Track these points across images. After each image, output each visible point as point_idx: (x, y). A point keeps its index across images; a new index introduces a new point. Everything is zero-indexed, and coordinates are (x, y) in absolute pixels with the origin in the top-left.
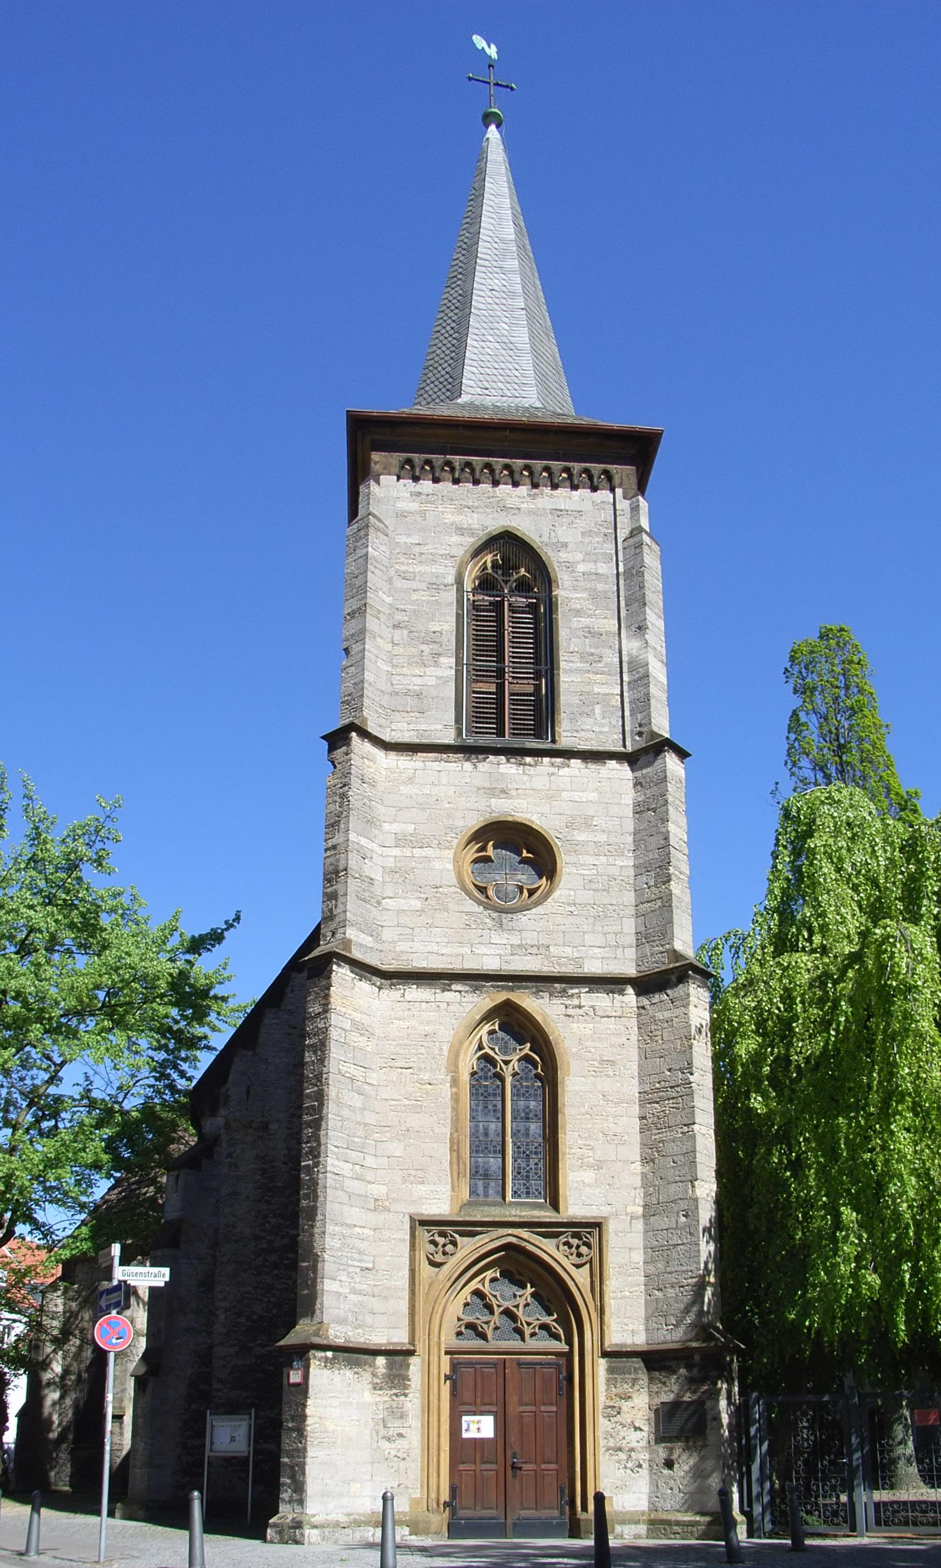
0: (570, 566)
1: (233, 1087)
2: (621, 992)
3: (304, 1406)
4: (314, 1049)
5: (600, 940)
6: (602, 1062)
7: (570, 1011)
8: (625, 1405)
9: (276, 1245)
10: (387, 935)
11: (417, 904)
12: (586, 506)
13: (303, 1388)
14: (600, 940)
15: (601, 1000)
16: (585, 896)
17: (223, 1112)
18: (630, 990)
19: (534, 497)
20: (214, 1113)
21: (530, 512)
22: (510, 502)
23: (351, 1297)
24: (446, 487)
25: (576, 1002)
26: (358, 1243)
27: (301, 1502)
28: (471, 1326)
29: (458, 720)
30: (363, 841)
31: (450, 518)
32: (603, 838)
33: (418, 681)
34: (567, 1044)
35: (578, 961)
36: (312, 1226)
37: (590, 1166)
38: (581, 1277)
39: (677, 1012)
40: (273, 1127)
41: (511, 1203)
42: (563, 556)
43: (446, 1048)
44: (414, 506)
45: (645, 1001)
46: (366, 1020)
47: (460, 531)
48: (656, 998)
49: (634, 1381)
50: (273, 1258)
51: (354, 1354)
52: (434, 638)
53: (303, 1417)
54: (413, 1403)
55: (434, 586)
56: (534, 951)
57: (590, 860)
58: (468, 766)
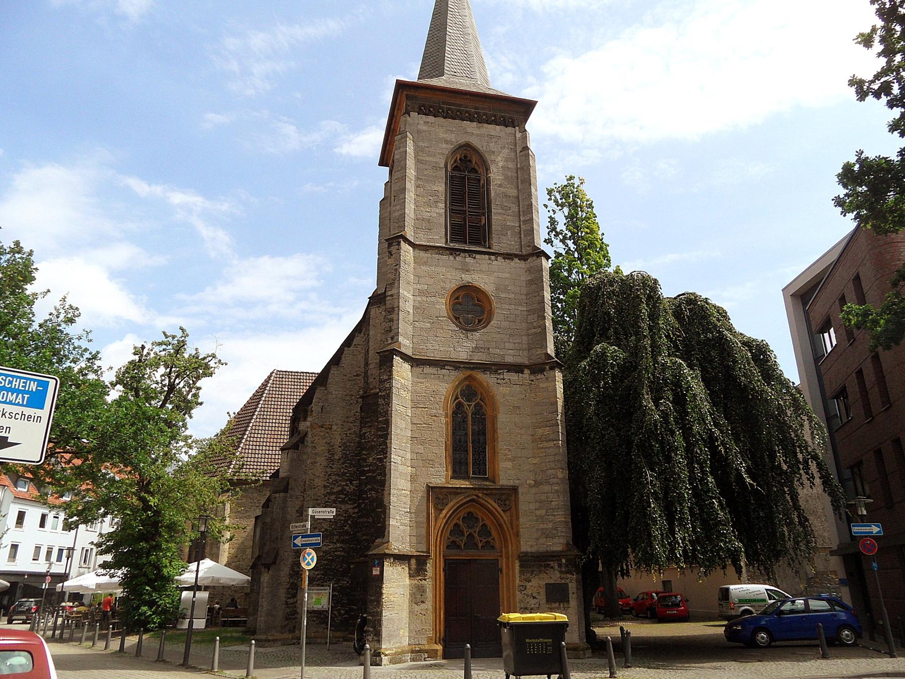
1: (315, 406)
2: (522, 372)
3: (381, 588)
4: (384, 397)
5: (511, 346)
6: (514, 407)
7: (499, 381)
8: (528, 585)
9: (335, 491)
12: (502, 134)
13: (380, 578)
14: (511, 346)
15: (514, 377)
16: (505, 324)
17: (309, 419)
18: (526, 371)
19: (479, 128)
20: (305, 420)
21: (477, 135)
22: (469, 130)
24: (440, 120)
25: (502, 377)
27: (379, 641)
28: (453, 542)
29: (446, 235)
30: (405, 293)
31: (442, 135)
32: (512, 296)
34: (498, 398)
35: (503, 356)
36: (383, 490)
37: (510, 460)
38: (505, 517)
39: (549, 384)
40: (334, 427)
42: (493, 157)
43: (443, 398)
44: (425, 128)
45: (532, 377)
47: (447, 142)
48: (539, 376)
49: (532, 572)
50: (333, 497)
51: (400, 558)
52: (435, 194)
53: (381, 594)
54: (428, 584)
55: (435, 168)
56: (482, 350)
57: (507, 307)
58: (451, 258)
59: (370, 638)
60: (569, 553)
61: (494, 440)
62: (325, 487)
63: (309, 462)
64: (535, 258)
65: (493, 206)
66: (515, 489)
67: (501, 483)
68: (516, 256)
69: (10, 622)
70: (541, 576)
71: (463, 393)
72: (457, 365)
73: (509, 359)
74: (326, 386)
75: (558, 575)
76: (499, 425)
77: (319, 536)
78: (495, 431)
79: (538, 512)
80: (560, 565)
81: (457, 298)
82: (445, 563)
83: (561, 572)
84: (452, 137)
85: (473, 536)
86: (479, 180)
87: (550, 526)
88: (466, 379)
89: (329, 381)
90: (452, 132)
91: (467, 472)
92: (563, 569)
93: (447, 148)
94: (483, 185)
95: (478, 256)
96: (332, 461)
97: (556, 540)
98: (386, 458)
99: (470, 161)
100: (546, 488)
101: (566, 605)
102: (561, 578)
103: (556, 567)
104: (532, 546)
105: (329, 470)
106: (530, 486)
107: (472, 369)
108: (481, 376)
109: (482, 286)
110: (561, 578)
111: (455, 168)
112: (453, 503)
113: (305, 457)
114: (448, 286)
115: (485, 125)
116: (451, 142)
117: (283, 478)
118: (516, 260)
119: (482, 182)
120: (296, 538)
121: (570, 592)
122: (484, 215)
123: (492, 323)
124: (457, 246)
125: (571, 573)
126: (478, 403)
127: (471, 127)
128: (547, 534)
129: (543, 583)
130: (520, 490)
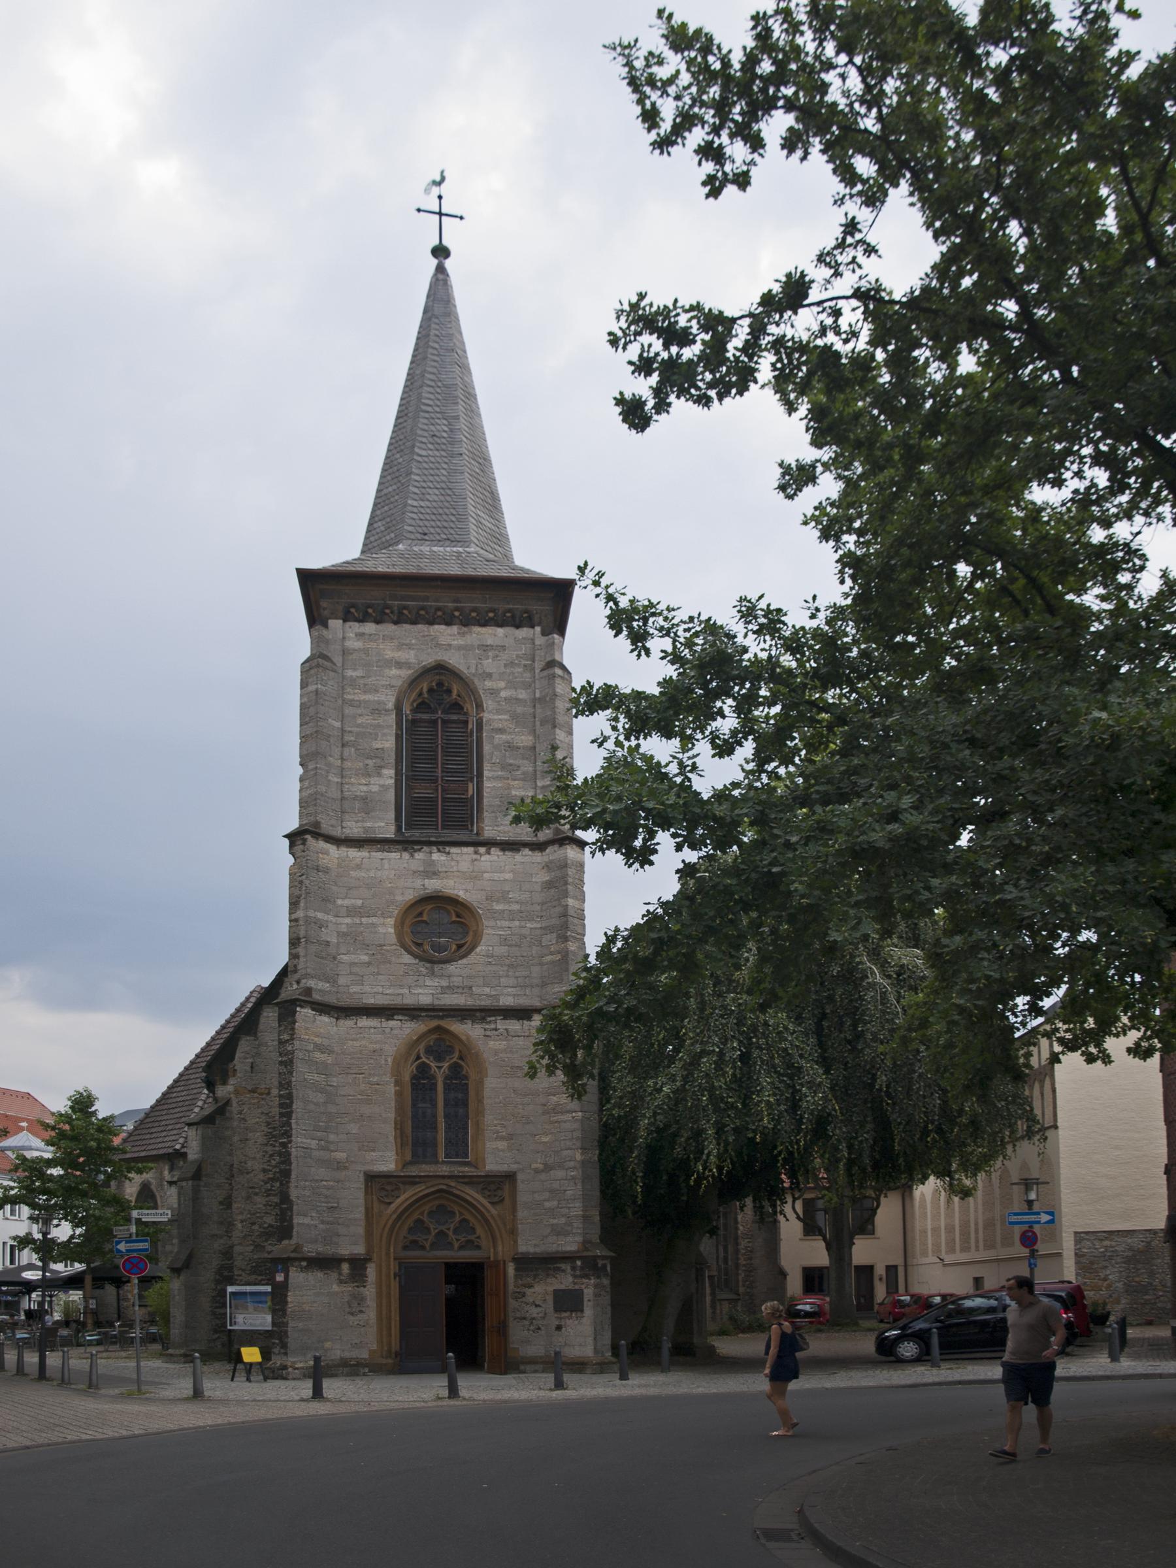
0: (494, 692)
1: (241, 1061)
5: (512, 981)
7: (488, 1033)
8: (529, 1291)
10: (342, 981)
11: (365, 958)
14: (512, 981)
15: (514, 1025)
16: (502, 950)
17: (232, 1081)
19: (463, 634)
20: (225, 1083)
21: (459, 648)
22: (443, 640)
23: (321, 1226)
24: (389, 628)
25: (493, 1026)
26: (324, 1191)
31: (389, 654)
32: (516, 907)
33: (365, 788)
34: (485, 1055)
35: (496, 997)
36: (288, 1182)
37: (503, 1138)
41: (443, 1162)
44: (358, 644)
46: (326, 1042)
47: (399, 665)
49: (535, 1276)
54: (369, 1292)
56: (460, 990)
57: (507, 924)
58: (406, 855)
59: (276, 1350)
60: (586, 1254)
61: (480, 1112)
62: (264, 1171)
63: (236, 1139)
64: (556, 847)
65: (487, 766)
66: (510, 1177)
67: (488, 1168)
68: (525, 845)
69: (1114, 1358)
70: (549, 1280)
71: (429, 1051)
72: (413, 1012)
73: (507, 1001)
74: (255, 1034)
75: (571, 1279)
76: (487, 1093)
77: (146, 1241)
78: (480, 1101)
79: (547, 1204)
80: (574, 1268)
81: (421, 914)
82: (473, 1265)
83: (575, 1276)
84: (410, 656)
85: (446, 1235)
86: (466, 722)
87: (563, 1220)
88: (431, 1031)
89: (261, 1027)
90: (410, 646)
91: (435, 1155)
92: (578, 1273)
93: (398, 676)
94: (472, 730)
95: (454, 850)
96: (274, 1136)
97: (569, 1238)
98: (290, 1142)
99: (449, 691)
100: (560, 1174)
101: (579, 1314)
102: (575, 1284)
103: (569, 1270)
104: (535, 1245)
105: (269, 1149)
106: (537, 1171)
107: (442, 1018)
108: (459, 1028)
109: (461, 894)
110: (575, 1284)
111: (422, 706)
112: (407, 1195)
113: (228, 1133)
114: (399, 898)
115: (477, 629)
116: (407, 665)
117: (192, 1162)
118: (526, 851)
119: (470, 726)
120: (118, 1243)
121: (586, 1300)
122: (472, 781)
123: (478, 949)
124: (416, 834)
125: (587, 1276)
126: (456, 1063)
127: (445, 633)
128: (558, 1232)
129: (550, 1289)
130: (520, 1177)
